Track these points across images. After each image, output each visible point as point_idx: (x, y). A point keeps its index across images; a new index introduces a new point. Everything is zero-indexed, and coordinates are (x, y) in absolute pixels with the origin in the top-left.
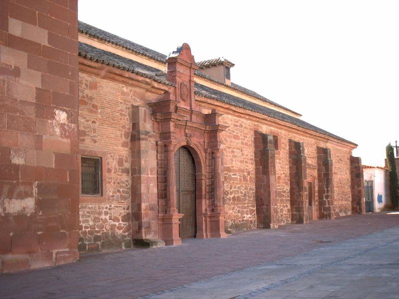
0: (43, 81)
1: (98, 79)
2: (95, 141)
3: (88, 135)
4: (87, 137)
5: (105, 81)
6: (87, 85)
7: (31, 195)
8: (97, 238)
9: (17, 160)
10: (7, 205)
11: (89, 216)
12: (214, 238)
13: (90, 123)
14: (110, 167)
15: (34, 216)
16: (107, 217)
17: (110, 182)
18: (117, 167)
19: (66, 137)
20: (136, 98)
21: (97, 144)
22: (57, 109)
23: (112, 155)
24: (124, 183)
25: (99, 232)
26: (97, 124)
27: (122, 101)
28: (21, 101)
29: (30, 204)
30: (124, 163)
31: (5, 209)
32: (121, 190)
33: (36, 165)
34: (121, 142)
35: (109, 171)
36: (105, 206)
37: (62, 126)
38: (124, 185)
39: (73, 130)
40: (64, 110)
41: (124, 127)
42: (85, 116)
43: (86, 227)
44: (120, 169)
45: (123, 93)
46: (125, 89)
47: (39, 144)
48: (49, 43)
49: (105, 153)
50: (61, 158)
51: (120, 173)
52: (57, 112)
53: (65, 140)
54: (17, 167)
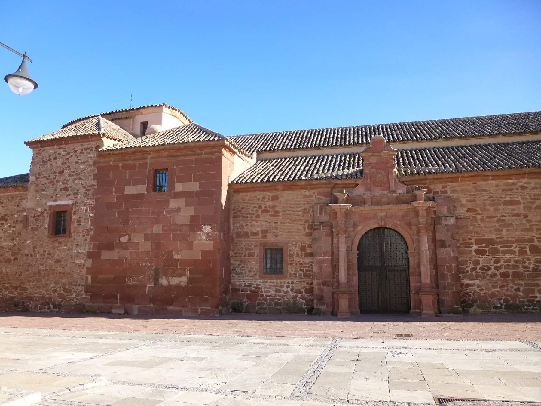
0: (195, 211)
1: (278, 193)
2: (276, 236)
3: (270, 233)
4: (269, 234)
5: (286, 192)
6: (269, 199)
7: (185, 275)
8: (277, 304)
9: (176, 257)
10: (170, 280)
11: (270, 288)
12: (191, 351)
13: (272, 224)
14: (292, 253)
15: (186, 286)
16: (289, 290)
17: (291, 264)
18: (300, 252)
19: (210, 240)
20: (321, 197)
21: (278, 238)
22: (203, 225)
23: (294, 243)
24: (308, 264)
25: (279, 300)
26: (279, 223)
27: (304, 203)
28: (181, 225)
29: (184, 280)
30: (307, 249)
31: (169, 282)
32: (304, 269)
33: (188, 258)
34: (304, 232)
35: (291, 256)
36: (287, 281)
37: (208, 234)
38: (309, 265)
39: (216, 235)
40: (208, 225)
41: (306, 221)
42: (267, 220)
43: (267, 296)
44: (302, 253)
45: (305, 196)
46: (307, 193)
47: (190, 246)
48: (231, 185)
49: (287, 244)
50: (205, 253)
51: (303, 257)
52: (204, 227)
53: (210, 242)
54: (177, 260)
